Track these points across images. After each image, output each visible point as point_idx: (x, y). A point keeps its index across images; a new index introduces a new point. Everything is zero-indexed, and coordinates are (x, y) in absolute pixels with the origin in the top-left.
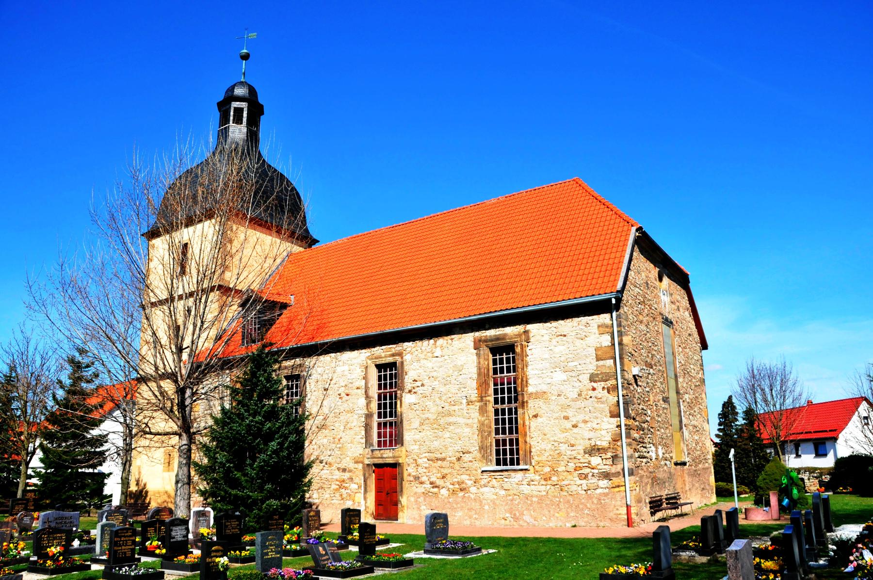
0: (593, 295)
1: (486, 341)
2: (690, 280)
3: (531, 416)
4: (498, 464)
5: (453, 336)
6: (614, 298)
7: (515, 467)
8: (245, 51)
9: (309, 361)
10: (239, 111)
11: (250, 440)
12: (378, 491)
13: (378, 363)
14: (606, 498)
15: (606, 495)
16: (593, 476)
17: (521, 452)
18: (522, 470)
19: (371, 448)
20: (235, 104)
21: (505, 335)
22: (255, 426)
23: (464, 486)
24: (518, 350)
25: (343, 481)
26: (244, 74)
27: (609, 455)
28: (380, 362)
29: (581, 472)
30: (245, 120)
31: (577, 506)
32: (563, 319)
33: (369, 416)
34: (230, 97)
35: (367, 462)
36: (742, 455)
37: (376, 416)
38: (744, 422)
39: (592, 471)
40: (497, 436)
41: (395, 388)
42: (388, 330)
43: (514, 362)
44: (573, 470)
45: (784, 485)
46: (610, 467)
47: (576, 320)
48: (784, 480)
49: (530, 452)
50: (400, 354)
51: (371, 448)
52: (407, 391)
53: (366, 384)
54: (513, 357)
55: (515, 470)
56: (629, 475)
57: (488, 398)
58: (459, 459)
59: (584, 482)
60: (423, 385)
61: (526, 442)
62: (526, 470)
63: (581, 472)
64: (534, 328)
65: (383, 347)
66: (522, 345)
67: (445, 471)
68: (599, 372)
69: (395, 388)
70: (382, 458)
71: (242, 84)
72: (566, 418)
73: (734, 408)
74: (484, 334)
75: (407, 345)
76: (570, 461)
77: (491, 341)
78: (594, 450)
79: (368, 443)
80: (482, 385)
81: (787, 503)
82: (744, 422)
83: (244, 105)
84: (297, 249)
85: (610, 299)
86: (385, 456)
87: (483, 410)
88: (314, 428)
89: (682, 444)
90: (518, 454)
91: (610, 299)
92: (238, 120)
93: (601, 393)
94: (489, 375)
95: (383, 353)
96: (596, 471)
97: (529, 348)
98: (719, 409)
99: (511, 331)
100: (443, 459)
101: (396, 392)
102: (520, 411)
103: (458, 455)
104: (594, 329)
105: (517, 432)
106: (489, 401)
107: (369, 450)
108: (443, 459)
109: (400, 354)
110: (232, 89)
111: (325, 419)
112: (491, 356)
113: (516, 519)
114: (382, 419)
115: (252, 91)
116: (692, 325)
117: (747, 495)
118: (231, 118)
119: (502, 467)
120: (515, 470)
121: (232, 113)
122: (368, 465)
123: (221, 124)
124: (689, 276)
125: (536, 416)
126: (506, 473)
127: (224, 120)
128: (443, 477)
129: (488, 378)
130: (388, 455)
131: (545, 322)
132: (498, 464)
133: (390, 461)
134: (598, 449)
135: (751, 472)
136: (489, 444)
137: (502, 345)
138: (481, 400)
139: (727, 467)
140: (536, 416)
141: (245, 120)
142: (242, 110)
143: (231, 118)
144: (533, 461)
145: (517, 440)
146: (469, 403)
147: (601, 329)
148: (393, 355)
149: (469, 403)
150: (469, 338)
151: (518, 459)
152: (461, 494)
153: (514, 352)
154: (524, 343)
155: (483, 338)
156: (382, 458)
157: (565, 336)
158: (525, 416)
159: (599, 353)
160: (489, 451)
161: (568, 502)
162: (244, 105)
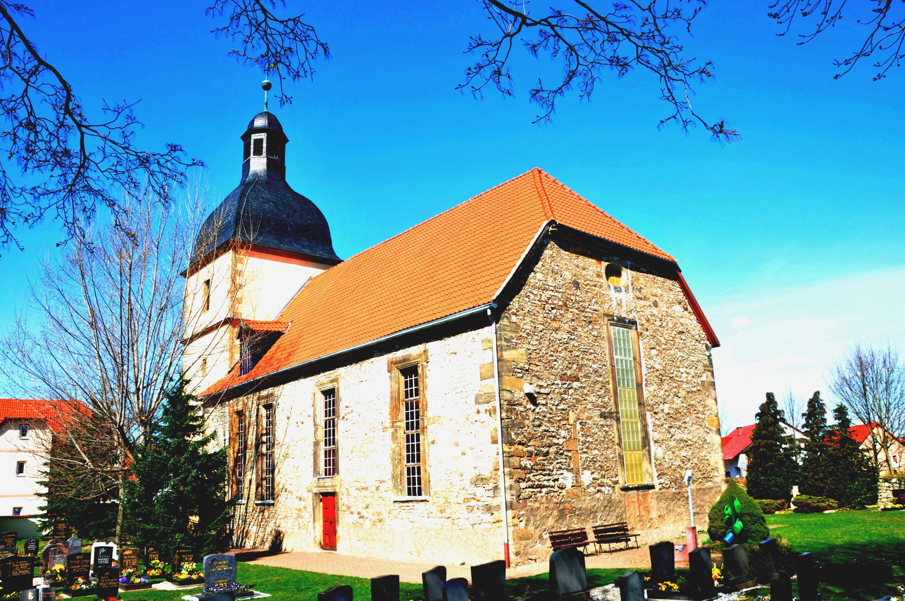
0: (474, 307)
1: (396, 363)
2: (680, 267)
3: (429, 442)
4: (409, 494)
5: (373, 359)
6: (489, 308)
7: (418, 498)
8: (266, 81)
9: (277, 390)
10: (259, 142)
11: (155, 476)
12: (325, 521)
13: (323, 389)
14: (488, 534)
15: (489, 530)
16: (478, 509)
17: (423, 482)
18: (422, 501)
19: (318, 477)
20: (255, 137)
21: (410, 355)
22: (159, 463)
23: (381, 517)
24: (420, 371)
25: (300, 510)
26: (266, 104)
27: (491, 486)
28: (326, 389)
29: (468, 504)
30: (264, 150)
31: (465, 542)
32: (454, 336)
33: (316, 444)
34: (252, 130)
35: (315, 490)
36: (828, 462)
37: (322, 444)
38: (837, 422)
39: (478, 503)
40: (408, 464)
41: (333, 415)
42: (324, 356)
43: (417, 384)
44: (462, 502)
45: (727, 516)
46: (492, 499)
47: (464, 335)
48: (727, 509)
49: (429, 481)
50: (335, 380)
51: (318, 477)
52: (341, 417)
53: (314, 411)
54: (416, 380)
55: (417, 501)
56: (90, 554)
57: (398, 424)
58: (377, 489)
59: (471, 515)
60: (352, 411)
61: (426, 471)
62: (425, 501)
63: (468, 504)
64: (433, 346)
65: (326, 373)
66: (422, 365)
67: (368, 501)
68: (482, 393)
69: (333, 415)
70: (324, 487)
71: (261, 114)
72: (457, 444)
73: (821, 406)
74: (395, 356)
75: (341, 370)
76: (460, 492)
77: (400, 362)
78: (480, 480)
79: (316, 471)
80: (395, 409)
81: (730, 539)
82: (837, 422)
83: (263, 136)
84: (314, 272)
85: (486, 311)
86: (326, 485)
87: (394, 437)
88: (281, 457)
89: (645, 464)
90: (420, 483)
91: (486, 311)
92: (258, 152)
93: (484, 416)
94: (399, 399)
95: (324, 379)
96: (480, 504)
97: (428, 368)
98: (805, 410)
99: (413, 352)
100: (366, 489)
101: (333, 420)
102: (421, 437)
103: (378, 484)
104: (479, 345)
105: (419, 461)
106: (399, 427)
107: (316, 478)
108: (366, 489)
109: (335, 380)
110: (252, 122)
111: (288, 448)
112: (402, 379)
113: (419, 554)
114: (328, 447)
115: (272, 119)
116: (691, 321)
117: (833, 511)
118: (252, 150)
119: (412, 498)
120: (417, 501)
121: (252, 146)
122: (316, 494)
123: (245, 158)
124: (678, 264)
125: (433, 443)
126: (410, 504)
127: (247, 154)
128: (367, 507)
129: (399, 402)
130: (329, 484)
131: (441, 339)
132: (409, 494)
133: (331, 491)
134: (482, 479)
135: (842, 483)
136: (399, 473)
137: (408, 366)
138: (393, 426)
139: (810, 477)
140: (433, 443)
141: (264, 150)
142: (261, 140)
143: (252, 150)
144: (431, 491)
145: (419, 468)
146: (385, 429)
147: (484, 344)
148: (332, 381)
149: (385, 429)
150: (381, 362)
151: (420, 489)
152: (379, 525)
153: (416, 374)
154: (425, 364)
155: (394, 360)
156: (324, 487)
157: (456, 353)
158: (425, 441)
159: (483, 371)
160: (399, 480)
161: (459, 537)
162: (263, 136)
